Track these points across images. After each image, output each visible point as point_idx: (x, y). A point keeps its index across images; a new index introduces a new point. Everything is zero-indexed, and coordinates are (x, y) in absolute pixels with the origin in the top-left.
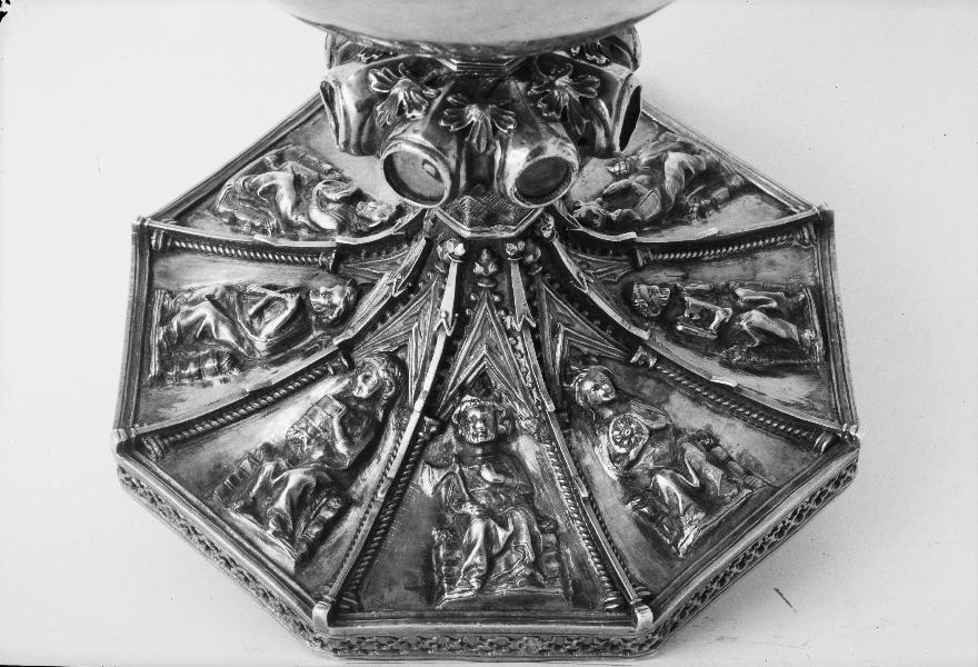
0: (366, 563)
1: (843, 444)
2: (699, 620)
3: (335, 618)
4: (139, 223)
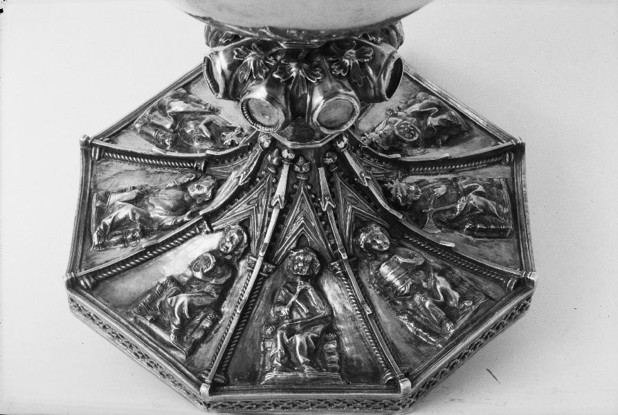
0: (229, 357)
1: (524, 285)
2: (428, 398)
3: (214, 389)
4: (84, 140)
